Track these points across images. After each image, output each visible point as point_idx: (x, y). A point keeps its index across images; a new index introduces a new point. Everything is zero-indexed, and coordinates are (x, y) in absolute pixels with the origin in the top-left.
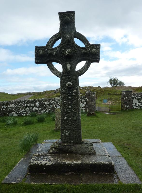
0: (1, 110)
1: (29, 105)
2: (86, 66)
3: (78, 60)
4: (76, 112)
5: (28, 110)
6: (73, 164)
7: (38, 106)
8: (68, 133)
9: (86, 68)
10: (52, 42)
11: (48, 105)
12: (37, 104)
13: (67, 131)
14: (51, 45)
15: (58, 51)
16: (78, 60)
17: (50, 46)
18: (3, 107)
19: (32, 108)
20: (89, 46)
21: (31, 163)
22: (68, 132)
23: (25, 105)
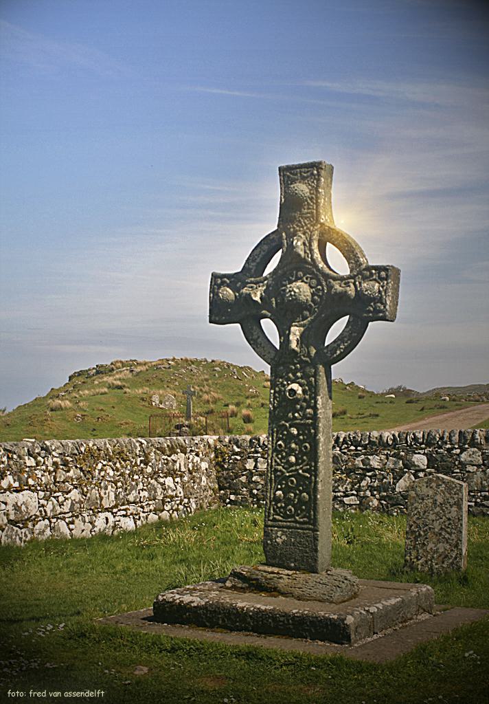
0: (243, 479)
1: (375, 462)
2: (345, 334)
3: (323, 315)
4: (308, 475)
5: (371, 488)
6: (252, 609)
7: (423, 470)
8: (284, 537)
9: (346, 339)
10: (258, 260)
11: (479, 466)
12: (420, 460)
13: (279, 533)
14: (254, 268)
15: (271, 288)
16: (323, 315)
17: (253, 271)
18: (250, 465)
19: (390, 479)
20: (361, 271)
21: (160, 598)
22: (282, 535)
23: (358, 461)
